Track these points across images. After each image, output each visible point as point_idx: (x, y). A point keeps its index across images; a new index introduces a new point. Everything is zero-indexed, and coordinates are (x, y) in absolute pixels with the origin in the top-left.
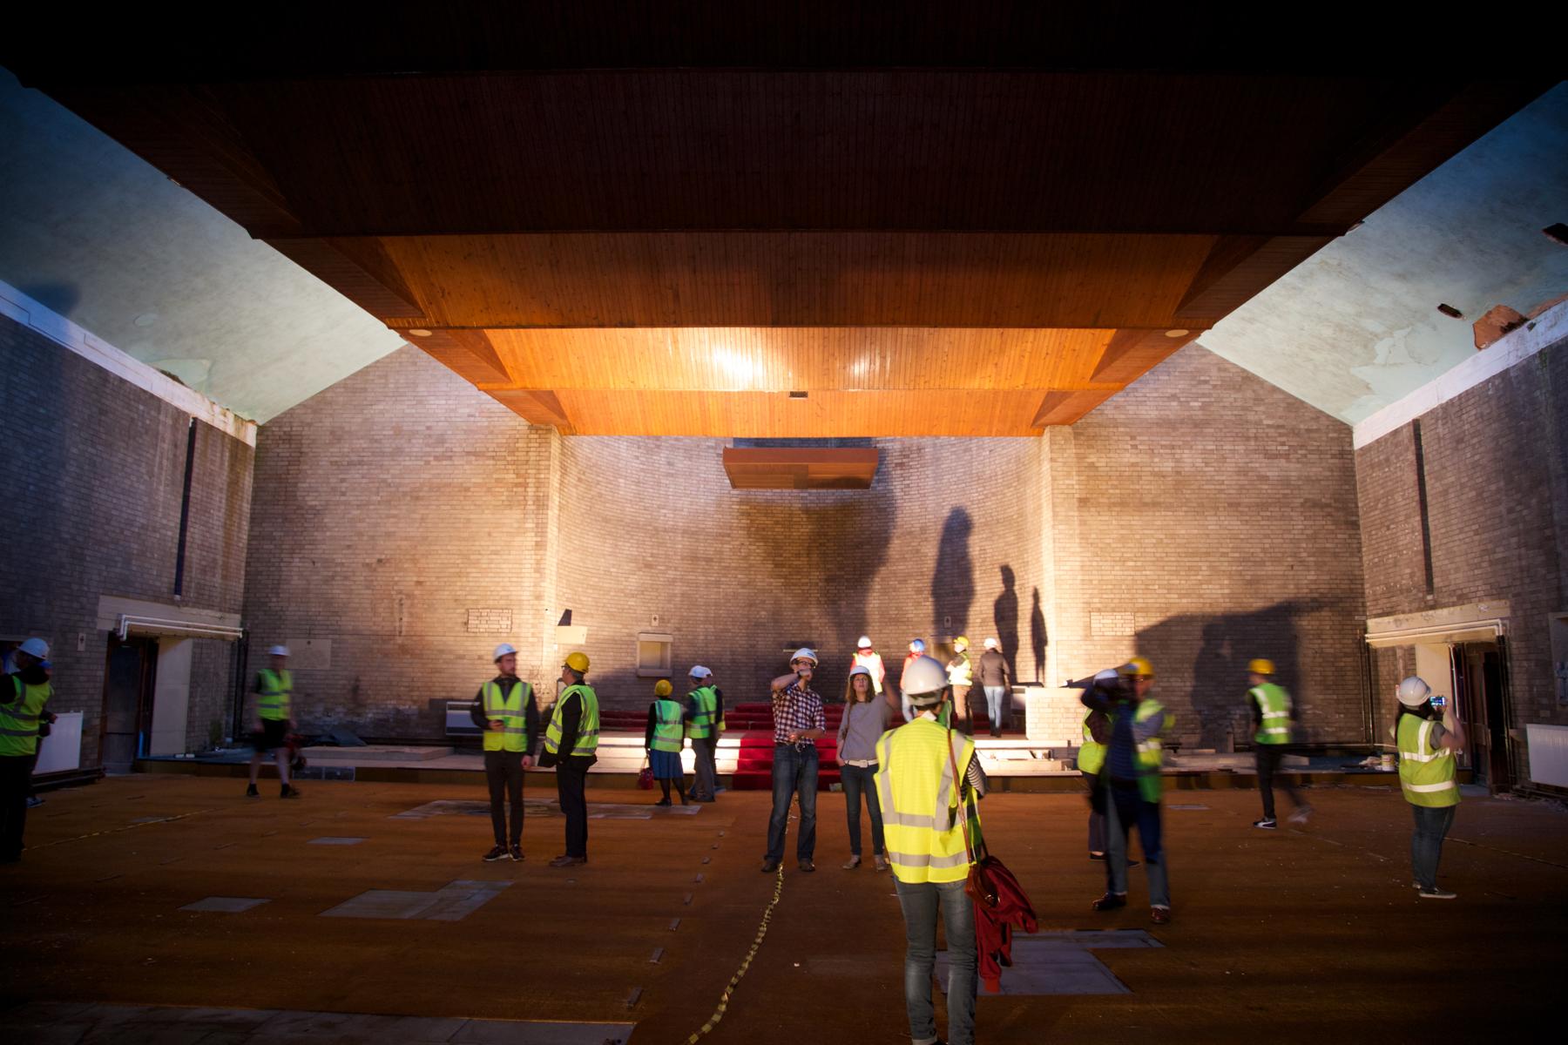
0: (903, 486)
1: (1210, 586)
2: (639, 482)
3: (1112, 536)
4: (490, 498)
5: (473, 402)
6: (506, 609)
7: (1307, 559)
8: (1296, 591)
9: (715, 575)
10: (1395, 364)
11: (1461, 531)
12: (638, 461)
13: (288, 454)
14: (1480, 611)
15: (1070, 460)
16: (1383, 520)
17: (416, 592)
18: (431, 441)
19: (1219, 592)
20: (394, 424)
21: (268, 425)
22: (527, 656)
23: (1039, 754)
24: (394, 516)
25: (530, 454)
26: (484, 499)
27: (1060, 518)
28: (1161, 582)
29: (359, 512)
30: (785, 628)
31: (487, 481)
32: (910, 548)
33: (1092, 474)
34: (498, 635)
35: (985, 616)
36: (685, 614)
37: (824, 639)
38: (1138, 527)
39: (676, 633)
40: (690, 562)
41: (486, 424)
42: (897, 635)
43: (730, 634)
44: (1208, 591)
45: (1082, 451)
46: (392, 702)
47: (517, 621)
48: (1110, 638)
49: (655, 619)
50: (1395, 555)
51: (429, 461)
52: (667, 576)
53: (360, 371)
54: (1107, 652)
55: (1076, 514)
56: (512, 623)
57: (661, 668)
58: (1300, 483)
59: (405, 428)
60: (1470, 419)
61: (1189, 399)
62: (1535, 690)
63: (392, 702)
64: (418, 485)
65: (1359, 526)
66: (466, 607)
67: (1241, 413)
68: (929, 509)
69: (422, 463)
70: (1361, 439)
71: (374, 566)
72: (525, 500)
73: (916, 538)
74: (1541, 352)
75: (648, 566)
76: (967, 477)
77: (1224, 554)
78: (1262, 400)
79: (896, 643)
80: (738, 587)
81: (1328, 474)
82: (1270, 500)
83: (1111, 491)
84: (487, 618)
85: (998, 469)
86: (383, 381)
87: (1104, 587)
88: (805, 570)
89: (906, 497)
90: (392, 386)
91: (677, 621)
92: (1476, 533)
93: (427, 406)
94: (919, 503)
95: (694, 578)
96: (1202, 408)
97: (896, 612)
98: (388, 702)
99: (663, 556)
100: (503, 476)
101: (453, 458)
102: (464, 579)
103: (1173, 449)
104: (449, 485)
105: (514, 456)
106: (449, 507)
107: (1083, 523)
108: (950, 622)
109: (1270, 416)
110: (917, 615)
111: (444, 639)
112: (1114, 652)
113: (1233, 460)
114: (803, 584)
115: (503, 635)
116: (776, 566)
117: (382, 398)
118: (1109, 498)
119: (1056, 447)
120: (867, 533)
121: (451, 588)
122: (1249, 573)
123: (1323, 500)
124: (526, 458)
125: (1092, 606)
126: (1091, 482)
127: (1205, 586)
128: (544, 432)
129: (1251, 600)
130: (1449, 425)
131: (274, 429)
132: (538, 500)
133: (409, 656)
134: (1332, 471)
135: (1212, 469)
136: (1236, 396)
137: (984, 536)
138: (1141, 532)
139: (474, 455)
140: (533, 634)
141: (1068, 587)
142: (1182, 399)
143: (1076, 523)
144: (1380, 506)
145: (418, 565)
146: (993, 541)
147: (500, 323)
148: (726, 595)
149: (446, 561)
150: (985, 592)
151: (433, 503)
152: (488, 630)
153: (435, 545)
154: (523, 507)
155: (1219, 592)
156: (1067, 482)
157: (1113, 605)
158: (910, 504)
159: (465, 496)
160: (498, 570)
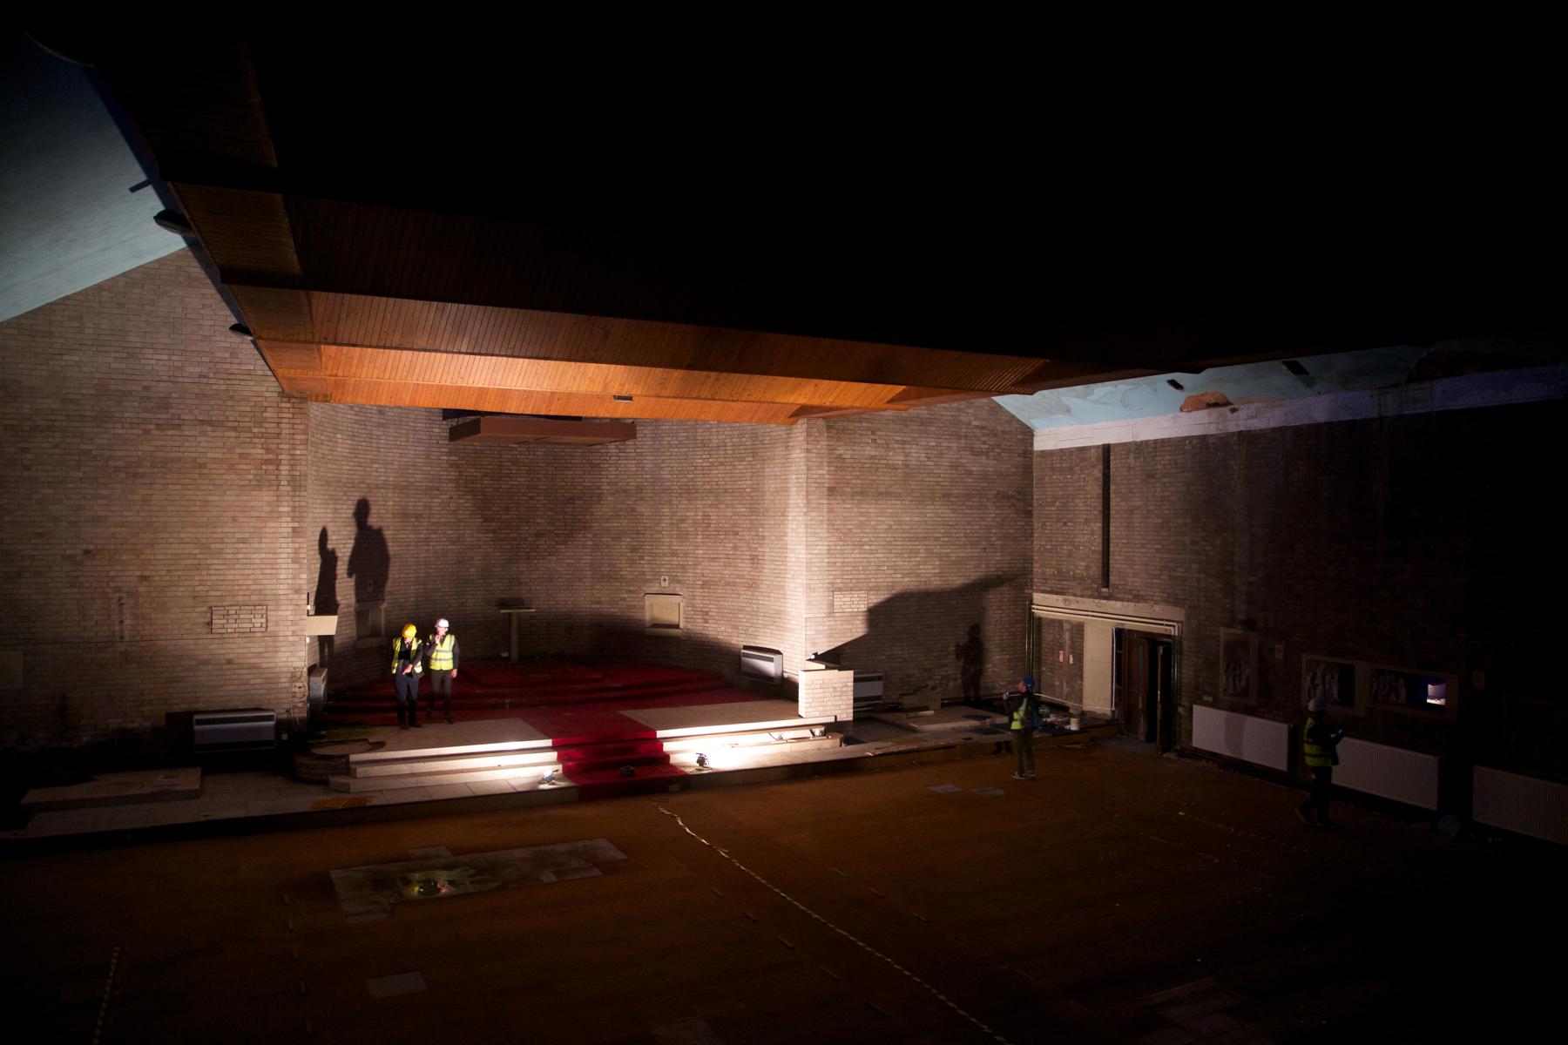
1: (926, 567)
2: (354, 436)
3: (854, 523)
4: (234, 477)
5: (205, 359)
7: (996, 543)
8: (986, 570)
9: (425, 532)
10: (1104, 403)
11: (1143, 546)
12: (353, 412)
15: (822, 451)
16: (1060, 516)
17: (141, 589)
19: (932, 571)
20: (96, 381)
23: (817, 731)
24: (104, 497)
25: (283, 426)
27: (812, 505)
28: (888, 564)
29: (52, 491)
31: (228, 456)
32: (625, 506)
33: (839, 465)
34: (251, 635)
35: (706, 579)
38: (874, 514)
41: (224, 387)
42: (609, 592)
43: (440, 594)
44: (924, 571)
45: (832, 443)
46: (116, 721)
47: (274, 619)
48: (849, 614)
49: (370, 584)
50: (1070, 548)
51: (150, 430)
53: (41, 309)
54: (845, 627)
55: (825, 502)
59: (112, 387)
60: (1163, 462)
63: (116, 721)
66: (209, 604)
67: (957, 414)
68: (646, 469)
69: (141, 432)
70: (1040, 444)
71: (78, 558)
72: (277, 479)
73: (632, 496)
74: (1240, 432)
76: (690, 442)
77: (937, 539)
79: (608, 599)
80: (447, 543)
81: (1014, 470)
82: (973, 492)
83: (854, 481)
84: (236, 617)
85: (728, 440)
86: (77, 324)
87: (845, 569)
88: (514, 524)
92: (1158, 551)
93: (143, 362)
94: (636, 462)
95: (404, 536)
100: (248, 451)
101: (183, 427)
102: (205, 572)
105: (262, 427)
106: (179, 487)
107: (831, 511)
108: (667, 582)
109: (977, 418)
111: (181, 642)
112: (851, 627)
114: (513, 539)
115: (256, 635)
116: (485, 520)
118: (852, 488)
119: (811, 438)
121: (186, 583)
122: (955, 555)
123: (1010, 493)
124: (278, 431)
125: (836, 586)
126: (839, 473)
127: (921, 567)
128: (299, 401)
129: (954, 578)
130: (1142, 459)
133: (135, 666)
134: (1017, 468)
137: (709, 502)
140: (293, 632)
141: (816, 569)
143: (826, 510)
144: (1057, 504)
147: (400, 344)
148: (436, 553)
150: (708, 556)
152: (237, 630)
155: (932, 571)
156: (819, 472)
157: (851, 585)
158: (624, 462)
159: (200, 474)
160: (248, 561)
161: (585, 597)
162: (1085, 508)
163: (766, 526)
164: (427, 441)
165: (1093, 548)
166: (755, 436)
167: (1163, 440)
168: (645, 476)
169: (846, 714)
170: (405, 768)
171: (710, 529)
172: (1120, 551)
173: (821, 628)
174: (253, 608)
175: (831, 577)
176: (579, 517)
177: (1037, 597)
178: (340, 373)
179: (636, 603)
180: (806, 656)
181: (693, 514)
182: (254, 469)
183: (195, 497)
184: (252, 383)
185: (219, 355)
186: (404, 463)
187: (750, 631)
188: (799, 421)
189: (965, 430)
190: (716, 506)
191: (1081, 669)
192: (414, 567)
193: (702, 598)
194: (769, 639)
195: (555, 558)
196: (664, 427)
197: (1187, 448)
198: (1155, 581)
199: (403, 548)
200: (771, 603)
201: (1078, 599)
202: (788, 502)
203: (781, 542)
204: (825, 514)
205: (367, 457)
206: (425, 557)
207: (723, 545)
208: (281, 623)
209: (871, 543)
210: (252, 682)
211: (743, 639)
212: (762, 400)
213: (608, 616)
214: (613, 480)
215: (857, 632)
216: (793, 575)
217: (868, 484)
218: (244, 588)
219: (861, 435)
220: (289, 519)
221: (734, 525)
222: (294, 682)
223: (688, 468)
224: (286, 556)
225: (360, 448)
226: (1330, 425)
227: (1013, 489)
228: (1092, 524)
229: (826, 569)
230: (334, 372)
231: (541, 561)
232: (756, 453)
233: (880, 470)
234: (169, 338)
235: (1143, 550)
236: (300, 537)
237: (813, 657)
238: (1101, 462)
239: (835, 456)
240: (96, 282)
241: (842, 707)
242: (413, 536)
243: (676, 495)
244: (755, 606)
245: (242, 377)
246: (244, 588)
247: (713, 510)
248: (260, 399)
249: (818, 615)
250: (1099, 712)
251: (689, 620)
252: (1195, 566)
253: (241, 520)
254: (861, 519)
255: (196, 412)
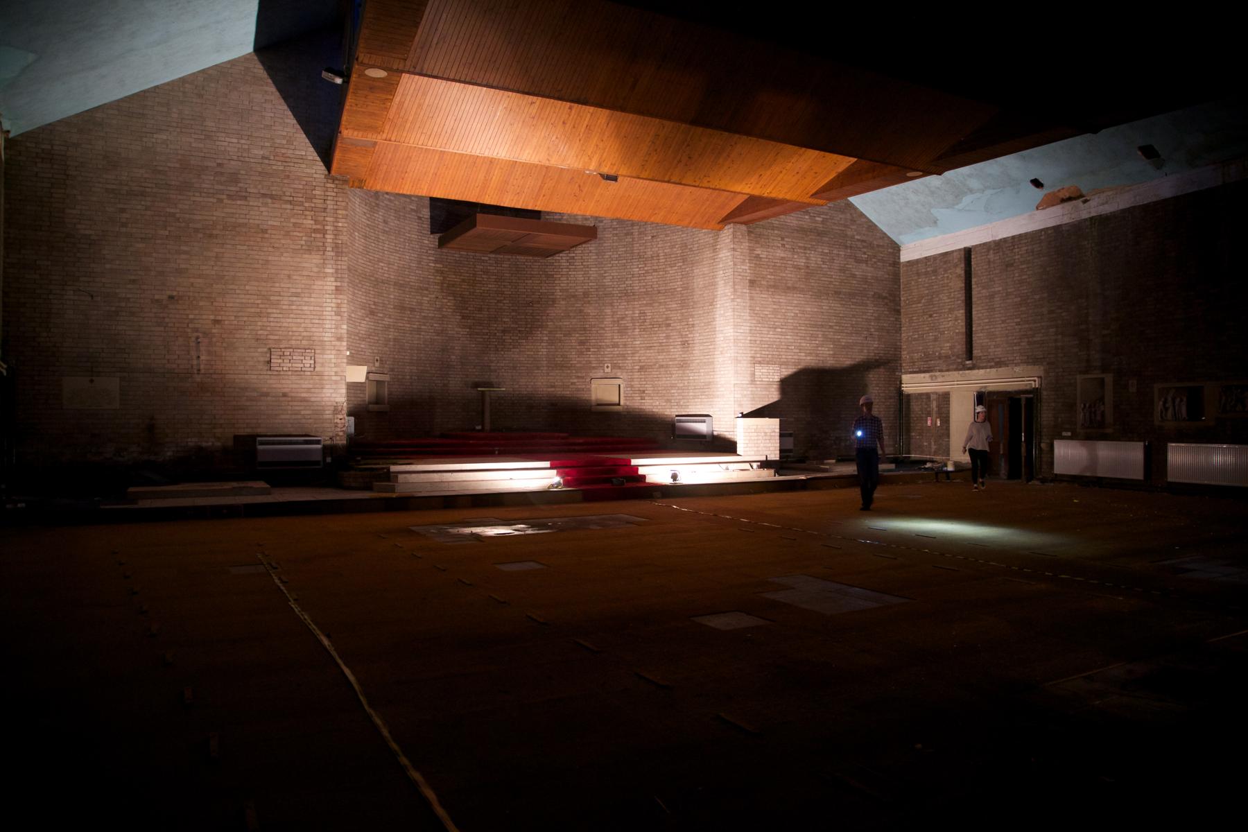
0: (568, 258)
1: (823, 349)
5: (267, 144)
6: (309, 349)
7: (874, 333)
9: (417, 323)
10: (969, 211)
11: (1003, 322)
13: (50, 175)
14: (1015, 372)
15: (745, 251)
17: (214, 331)
18: (223, 179)
19: (828, 353)
20: (179, 157)
21: (20, 139)
22: (331, 393)
23: (755, 465)
25: (328, 202)
26: (283, 241)
27: (738, 294)
28: (795, 344)
29: (144, 245)
30: (470, 370)
31: (284, 224)
32: (574, 308)
34: (302, 373)
35: (643, 364)
36: (396, 357)
37: (501, 380)
39: (391, 373)
40: (399, 311)
41: (281, 168)
44: (821, 352)
47: (320, 361)
52: (384, 322)
53: (137, 95)
54: (764, 393)
55: (748, 291)
56: (315, 362)
57: (377, 403)
58: (873, 281)
59: (192, 162)
61: (815, 215)
62: (1060, 419)
63: (193, 440)
64: (211, 223)
65: (900, 312)
66: (268, 347)
68: (591, 278)
70: (905, 257)
73: (580, 301)
74: (1091, 218)
75: (372, 313)
76: (628, 255)
77: (831, 327)
78: (855, 221)
80: (434, 334)
81: (887, 276)
82: (856, 292)
83: (769, 277)
84: (290, 357)
86: (165, 109)
87: (763, 346)
88: (486, 322)
89: (571, 267)
90: (176, 115)
91: (390, 363)
92: (1018, 324)
93: (218, 143)
94: (583, 273)
95: (402, 325)
96: (823, 222)
97: (562, 359)
98: (189, 440)
99: (381, 305)
100: (300, 221)
102: (265, 319)
103: (805, 250)
104: (244, 225)
106: (245, 247)
107: (752, 298)
108: (610, 369)
109: (859, 234)
110: (579, 362)
112: (768, 393)
113: (838, 262)
115: (306, 373)
116: (463, 317)
117: (163, 128)
118: (768, 281)
119: (737, 240)
120: (537, 294)
121: (250, 328)
124: (325, 206)
125: (757, 359)
128: (341, 182)
129: (844, 359)
130: (1001, 254)
131: (28, 144)
132: (337, 247)
133: (209, 394)
134: (889, 275)
135: (826, 266)
136: (840, 216)
137: (645, 302)
138: (785, 307)
139: (271, 199)
140: (336, 372)
142: (812, 214)
143: (748, 298)
144: (923, 301)
145: (215, 304)
146: (653, 306)
149: (244, 301)
150: (644, 345)
151: (228, 242)
152: (291, 369)
153: (233, 284)
154: (322, 253)
155: (828, 353)
156: (743, 267)
157: (768, 359)
158: (573, 273)
159: (262, 238)
160: (299, 312)
161: (542, 382)
162: (948, 301)
163: (696, 316)
164: (419, 250)
165: (957, 331)
166: (684, 246)
167: (1020, 235)
168: (590, 284)
169: (774, 455)
170: (436, 477)
171: (646, 324)
172: (983, 329)
173: (745, 392)
174: (303, 351)
175: (753, 352)
176: (538, 317)
177: (905, 378)
178: (393, 139)
179: (584, 386)
180: (735, 414)
181: (631, 312)
182: (306, 236)
183: (257, 257)
184: (304, 166)
185: (278, 141)
186: (402, 266)
187: (682, 403)
188: (726, 227)
189: (849, 242)
190: (651, 305)
191: (948, 429)
192: (409, 351)
193: (639, 380)
194: (699, 407)
195: (518, 350)
196: (606, 245)
197: (1043, 237)
198: (1015, 348)
199: (402, 334)
200: (701, 377)
201: (943, 373)
202: (716, 293)
203: (710, 327)
204: (747, 301)
205: (376, 256)
206: (418, 344)
207: (657, 335)
208: (327, 365)
209: (782, 327)
210: (302, 412)
211: (675, 410)
212: (717, 187)
213: (561, 397)
214: (564, 288)
215: (772, 398)
216: (721, 351)
217: (779, 280)
218: (297, 334)
219: (773, 240)
220: (333, 279)
221: (667, 319)
222: (336, 414)
223: (626, 276)
224: (330, 309)
225: (370, 247)
226: (1176, 199)
227: (886, 291)
228: (956, 312)
229: (749, 345)
230: (389, 136)
231: (506, 353)
232: (686, 258)
233: (788, 269)
234: (238, 125)
235: (1003, 325)
236: (341, 294)
237: (740, 415)
238: (963, 262)
239: (754, 255)
240: (180, 76)
241: (771, 449)
242: (409, 326)
243: (618, 298)
244: (686, 382)
245: (296, 161)
246: (297, 334)
247: (648, 308)
248: (311, 179)
249: (743, 382)
250: (963, 462)
251: (628, 398)
252: (1052, 330)
253: (295, 277)
254: (775, 307)
255: (260, 187)
